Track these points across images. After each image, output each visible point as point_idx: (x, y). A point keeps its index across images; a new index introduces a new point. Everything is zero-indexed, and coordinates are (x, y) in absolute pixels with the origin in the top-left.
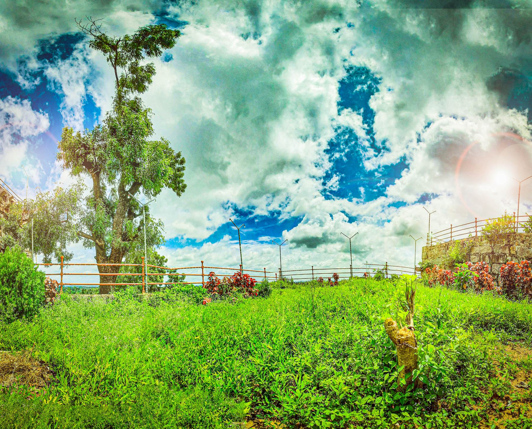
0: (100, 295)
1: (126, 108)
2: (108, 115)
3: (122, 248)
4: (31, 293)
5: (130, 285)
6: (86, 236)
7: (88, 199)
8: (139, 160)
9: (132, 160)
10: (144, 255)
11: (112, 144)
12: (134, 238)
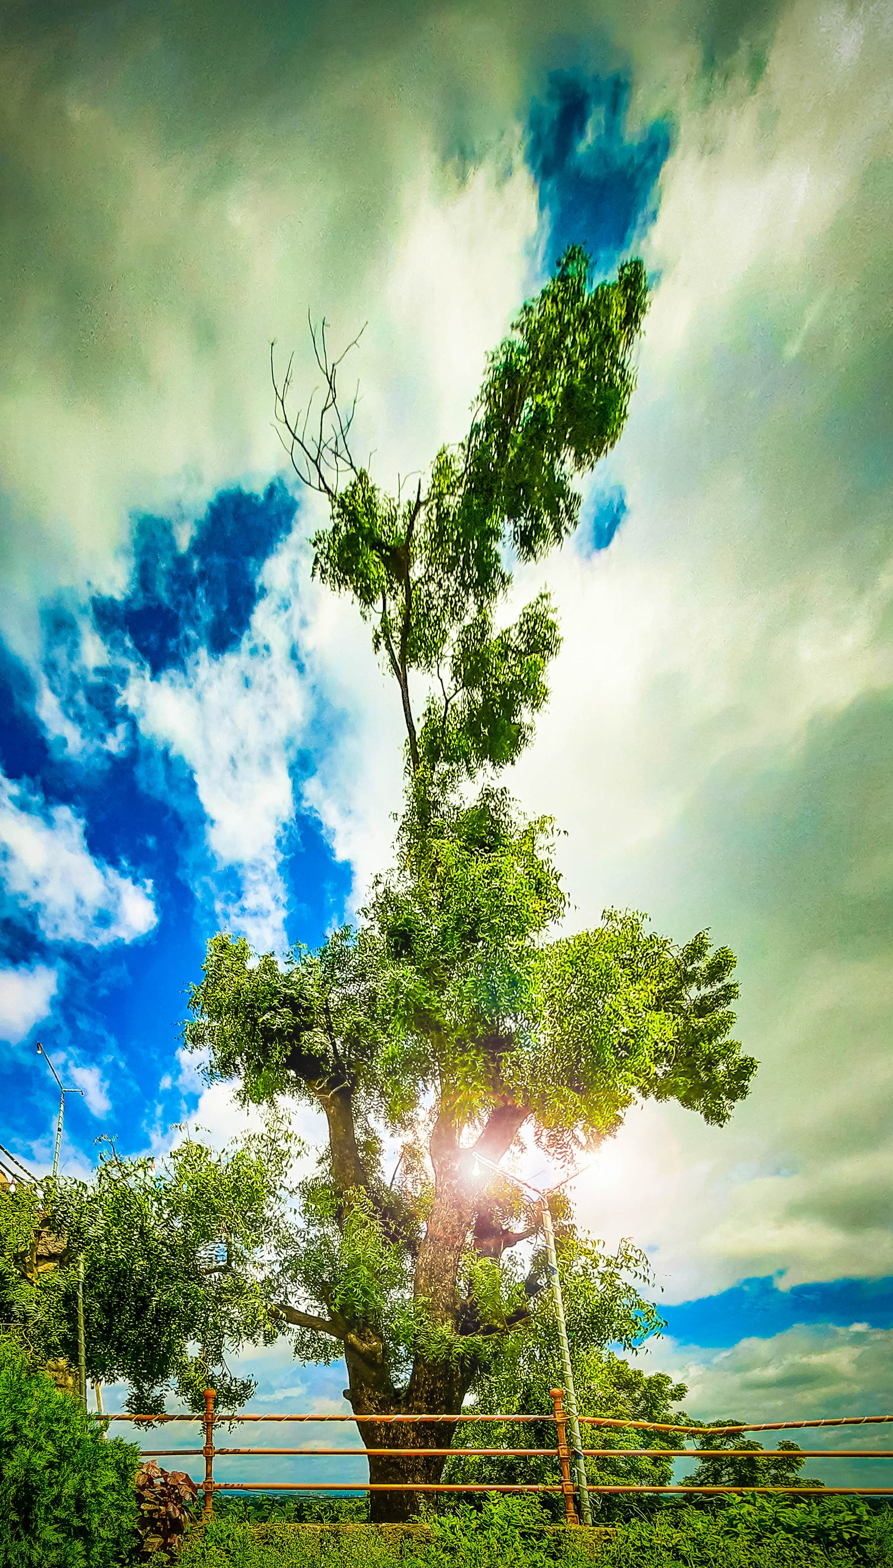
0: (372, 1527)
1: (447, 848)
2: (381, 888)
3: (461, 1358)
4: (76, 1522)
5: (504, 1492)
6: (304, 1321)
7: (309, 1191)
8: (509, 1022)
9: (480, 1031)
10: (562, 1378)
11: (398, 986)
12: (511, 1320)
